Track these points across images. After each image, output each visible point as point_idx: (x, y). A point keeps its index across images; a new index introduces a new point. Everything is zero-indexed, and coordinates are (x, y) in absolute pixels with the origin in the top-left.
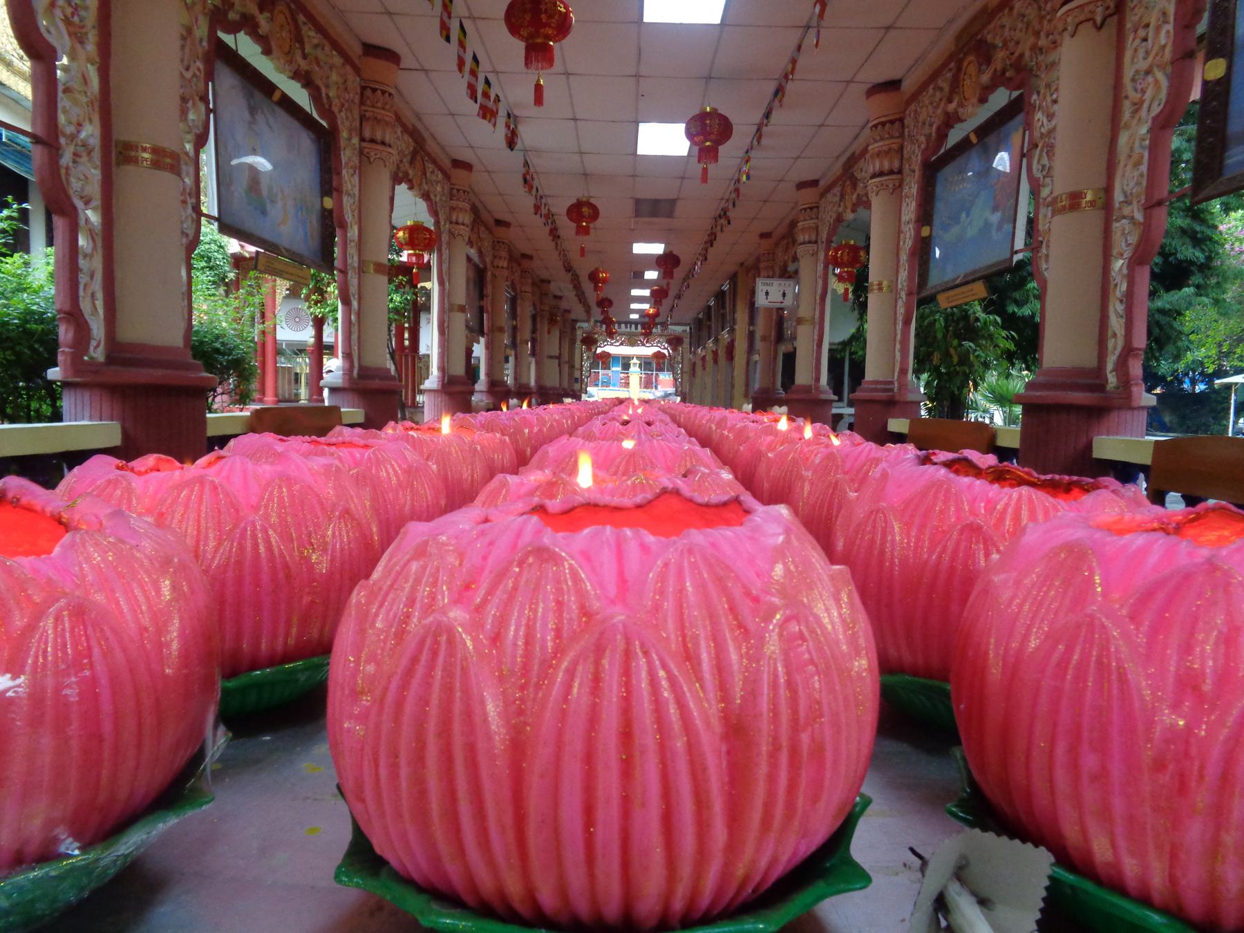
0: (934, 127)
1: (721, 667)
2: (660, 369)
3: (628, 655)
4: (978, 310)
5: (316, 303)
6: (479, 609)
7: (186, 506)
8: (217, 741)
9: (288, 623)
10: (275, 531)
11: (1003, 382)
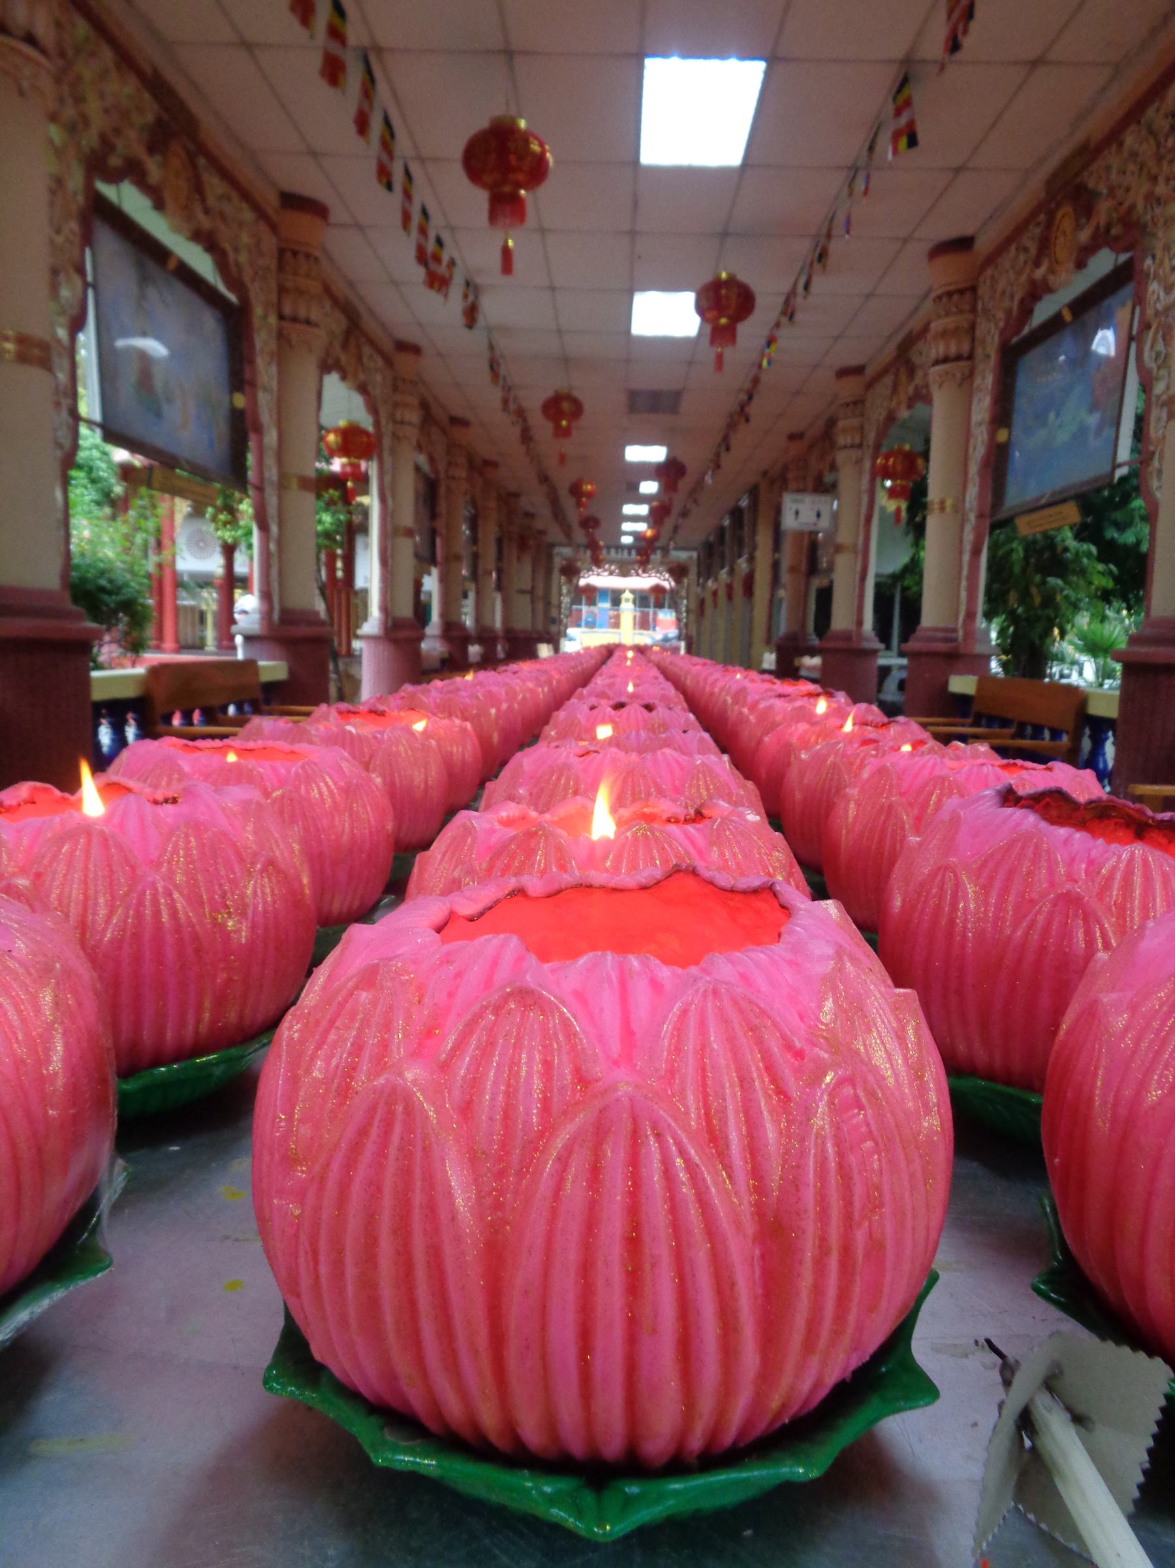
0: (1017, 298)
1: (753, 1148)
2: (659, 605)
3: (635, 1137)
4: (1068, 538)
5: (225, 524)
6: (445, 1067)
7: (70, 865)
8: (115, 1178)
9: (199, 1007)
10: (181, 893)
11: (1096, 626)
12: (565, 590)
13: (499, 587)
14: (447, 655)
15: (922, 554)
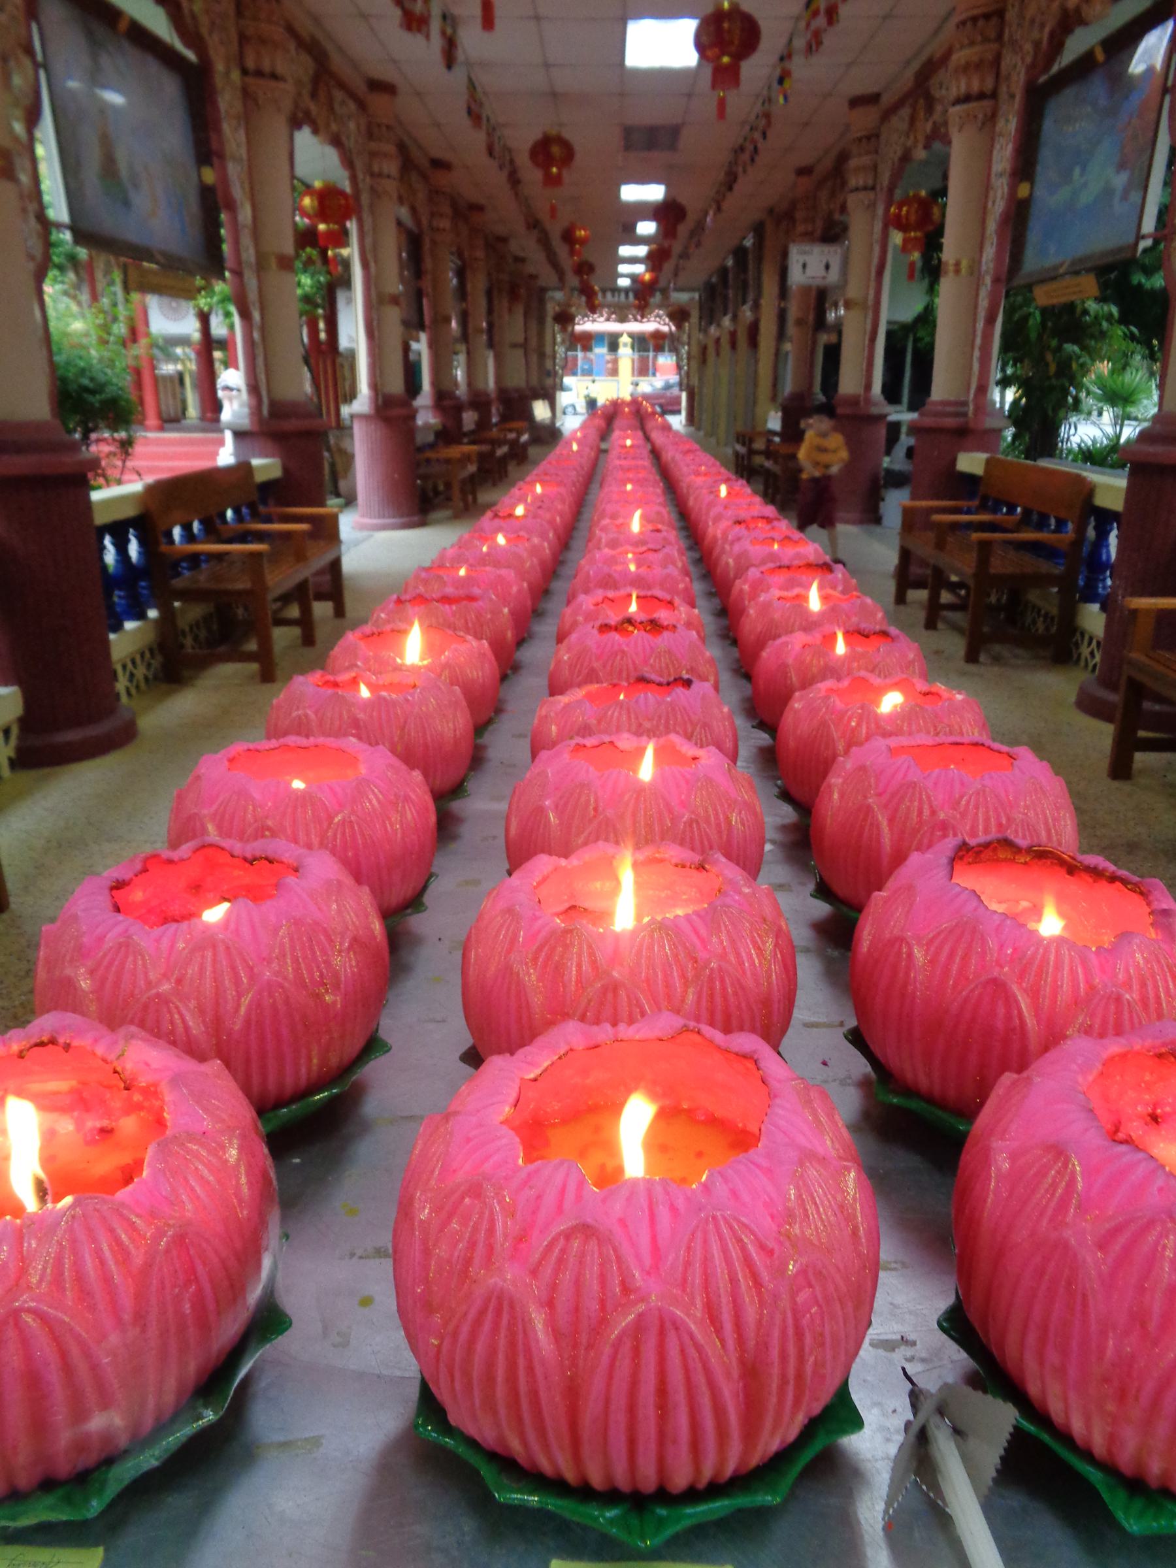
0: (1047, 30)
2: (659, 349)
3: (662, 1333)
6: (534, 1273)
9: (310, 1059)
12: (559, 338)
13: (491, 344)
14: (440, 427)
15: (937, 300)
